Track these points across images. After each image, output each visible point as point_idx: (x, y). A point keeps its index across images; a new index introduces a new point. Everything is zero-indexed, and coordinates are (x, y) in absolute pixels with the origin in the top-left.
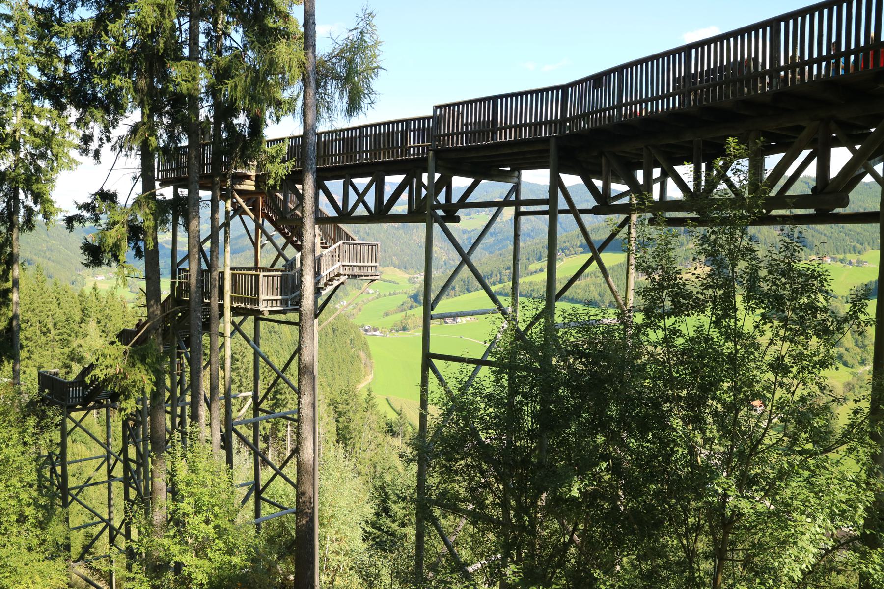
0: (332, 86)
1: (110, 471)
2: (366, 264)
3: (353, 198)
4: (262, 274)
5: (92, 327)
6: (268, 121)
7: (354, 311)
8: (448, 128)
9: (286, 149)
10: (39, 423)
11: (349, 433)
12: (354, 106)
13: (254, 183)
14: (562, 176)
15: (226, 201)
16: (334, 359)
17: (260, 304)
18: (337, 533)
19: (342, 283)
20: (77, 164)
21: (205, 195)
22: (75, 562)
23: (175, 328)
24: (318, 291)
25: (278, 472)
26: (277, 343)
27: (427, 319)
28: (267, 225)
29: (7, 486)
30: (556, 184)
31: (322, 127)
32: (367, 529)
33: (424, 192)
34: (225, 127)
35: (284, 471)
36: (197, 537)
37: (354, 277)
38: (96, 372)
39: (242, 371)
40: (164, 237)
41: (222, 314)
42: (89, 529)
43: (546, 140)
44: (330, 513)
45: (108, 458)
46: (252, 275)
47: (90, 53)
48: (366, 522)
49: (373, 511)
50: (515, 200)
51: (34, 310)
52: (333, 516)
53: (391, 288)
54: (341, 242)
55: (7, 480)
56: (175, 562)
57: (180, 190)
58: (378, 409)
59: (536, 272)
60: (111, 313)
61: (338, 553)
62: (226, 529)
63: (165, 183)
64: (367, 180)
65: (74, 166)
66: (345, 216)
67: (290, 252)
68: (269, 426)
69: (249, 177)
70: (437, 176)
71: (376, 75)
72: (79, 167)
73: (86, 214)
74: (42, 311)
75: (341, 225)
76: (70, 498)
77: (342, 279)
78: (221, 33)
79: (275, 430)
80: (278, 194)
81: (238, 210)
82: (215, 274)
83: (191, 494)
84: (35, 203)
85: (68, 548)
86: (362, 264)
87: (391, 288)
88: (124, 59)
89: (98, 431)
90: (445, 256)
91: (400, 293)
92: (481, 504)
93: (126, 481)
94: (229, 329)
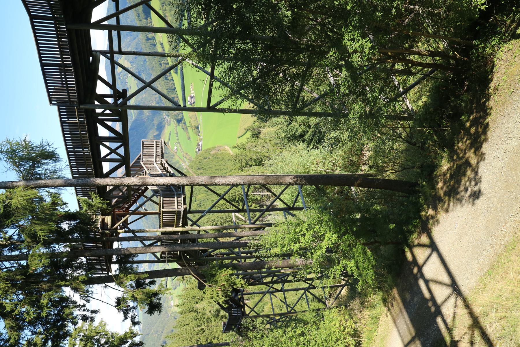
0: (39, 170)
1: (278, 291)
2: (155, 148)
3: (114, 156)
4: (162, 210)
5: (199, 306)
6: (66, 210)
7: (188, 157)
8: (64, 96)
9: (85, 198)
10: (251, 330)
11: (258, 159)
12: (52, 156)
13: (107, 217)
14: (93, 21)
15: (119, 233)
16: (216, 168)
17: (180, 210)
18: (313, 164)
19: (167, 162)
20: (102, 321)
21: (116, 245)
22: (326, 306)
23: (192, 257)
24: (171, 175)
25: (278, 197)
26: (203, 199)
27: (186, 109)
28: (133, 208)
29: (285, 343)
30: (98, 25)
31: (68, 175)
32: (311, 147)
33: (108, 112)
34: (71, 235)
35: (278, 194)
36: (313, 241)
37: (163, 155)
38: (221, 301)
39: (222, 221)
40: (145, 268)
41: (187, 232)
42: (310, 300)
43: (68, 30)
44: (302, 168)
45: (272, 293)
46: (163, 215)
47: (27, 320)
48: (308, 147)
49: (301, 144)
50: (110, 54)
51: (191, 338)
52: (304, 166)
53: (173, 136)
54: (141, 163)
55: (282, 343)
56: (326, 252)
57: (113, 261)
58: (244, 142)
59: (163, 48)
60: (191, 296)
61: (325, 163)
62: (309, 225)
63: (109, 269)
64: (102, 148)
65: (103, 323)
66: (124, 161)
67: (148, 194)
68: (254, 205)
69: (103, 220)
70: (96, 103)
71: (30, 142)
72: (104, 320)
73: (131, 314)
74: (191, 334)
75: (131, 165)
76: (293, 311)
77: (164, 162)
78: (9, 242)
79: (256, 201)
80: (113, 203)
81: (125, 225)
82: (165, 237)
83: (289, 244)
84: (127, 342)
85: (318, 310)
86: (155, 150)
87: (173, 136)
88: (30, 299)
89: (257, 298)
90: (148, 97)
91: (177, 130)
92: (296, 76)
93: (284, 282)
94: (195, 227)
